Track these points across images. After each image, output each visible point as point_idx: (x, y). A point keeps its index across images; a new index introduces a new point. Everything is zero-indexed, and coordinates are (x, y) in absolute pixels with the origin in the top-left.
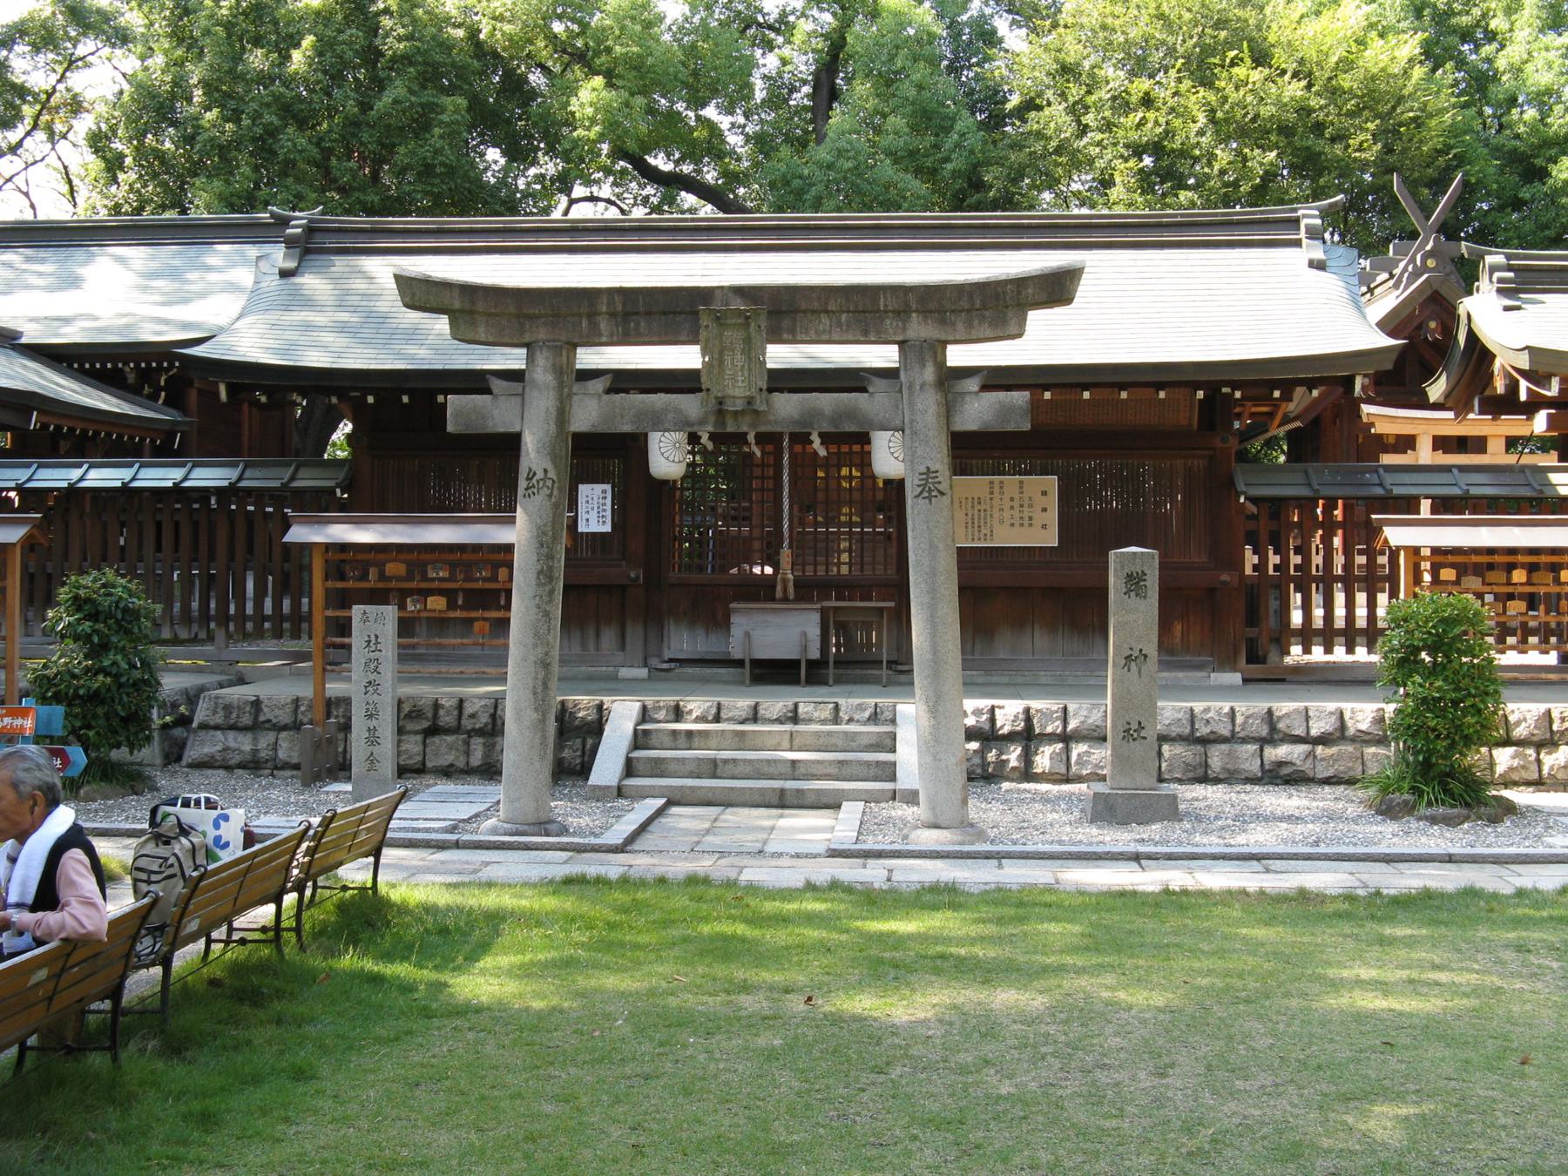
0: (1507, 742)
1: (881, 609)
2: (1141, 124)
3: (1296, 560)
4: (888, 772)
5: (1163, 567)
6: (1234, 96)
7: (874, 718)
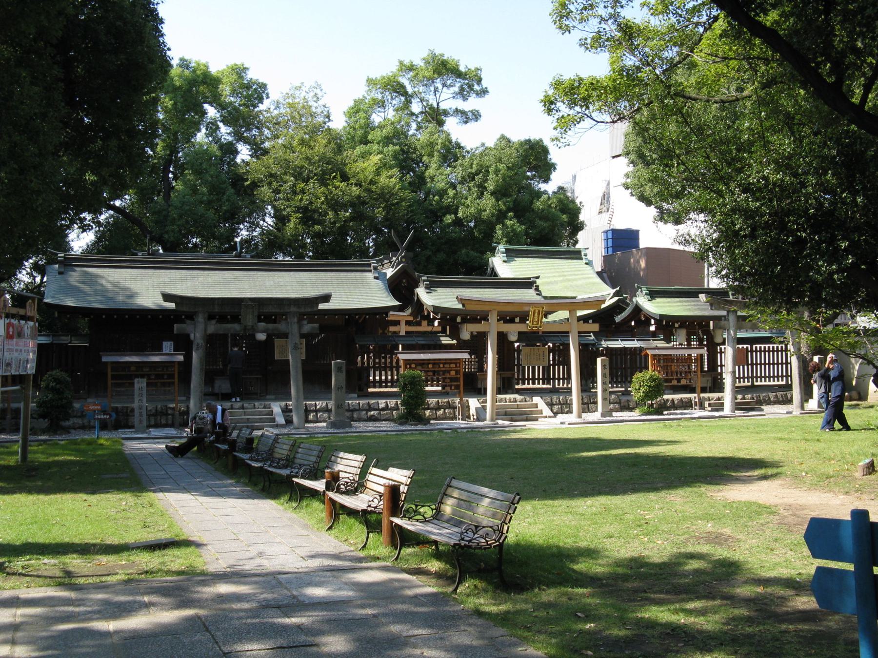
0: (428, 409)
1: (257, 378)
2: (301, 200)
3: (383, 360)
4: (274, 420)
5: (346, 365)
6: (335, 192)
7: (265, 407)
